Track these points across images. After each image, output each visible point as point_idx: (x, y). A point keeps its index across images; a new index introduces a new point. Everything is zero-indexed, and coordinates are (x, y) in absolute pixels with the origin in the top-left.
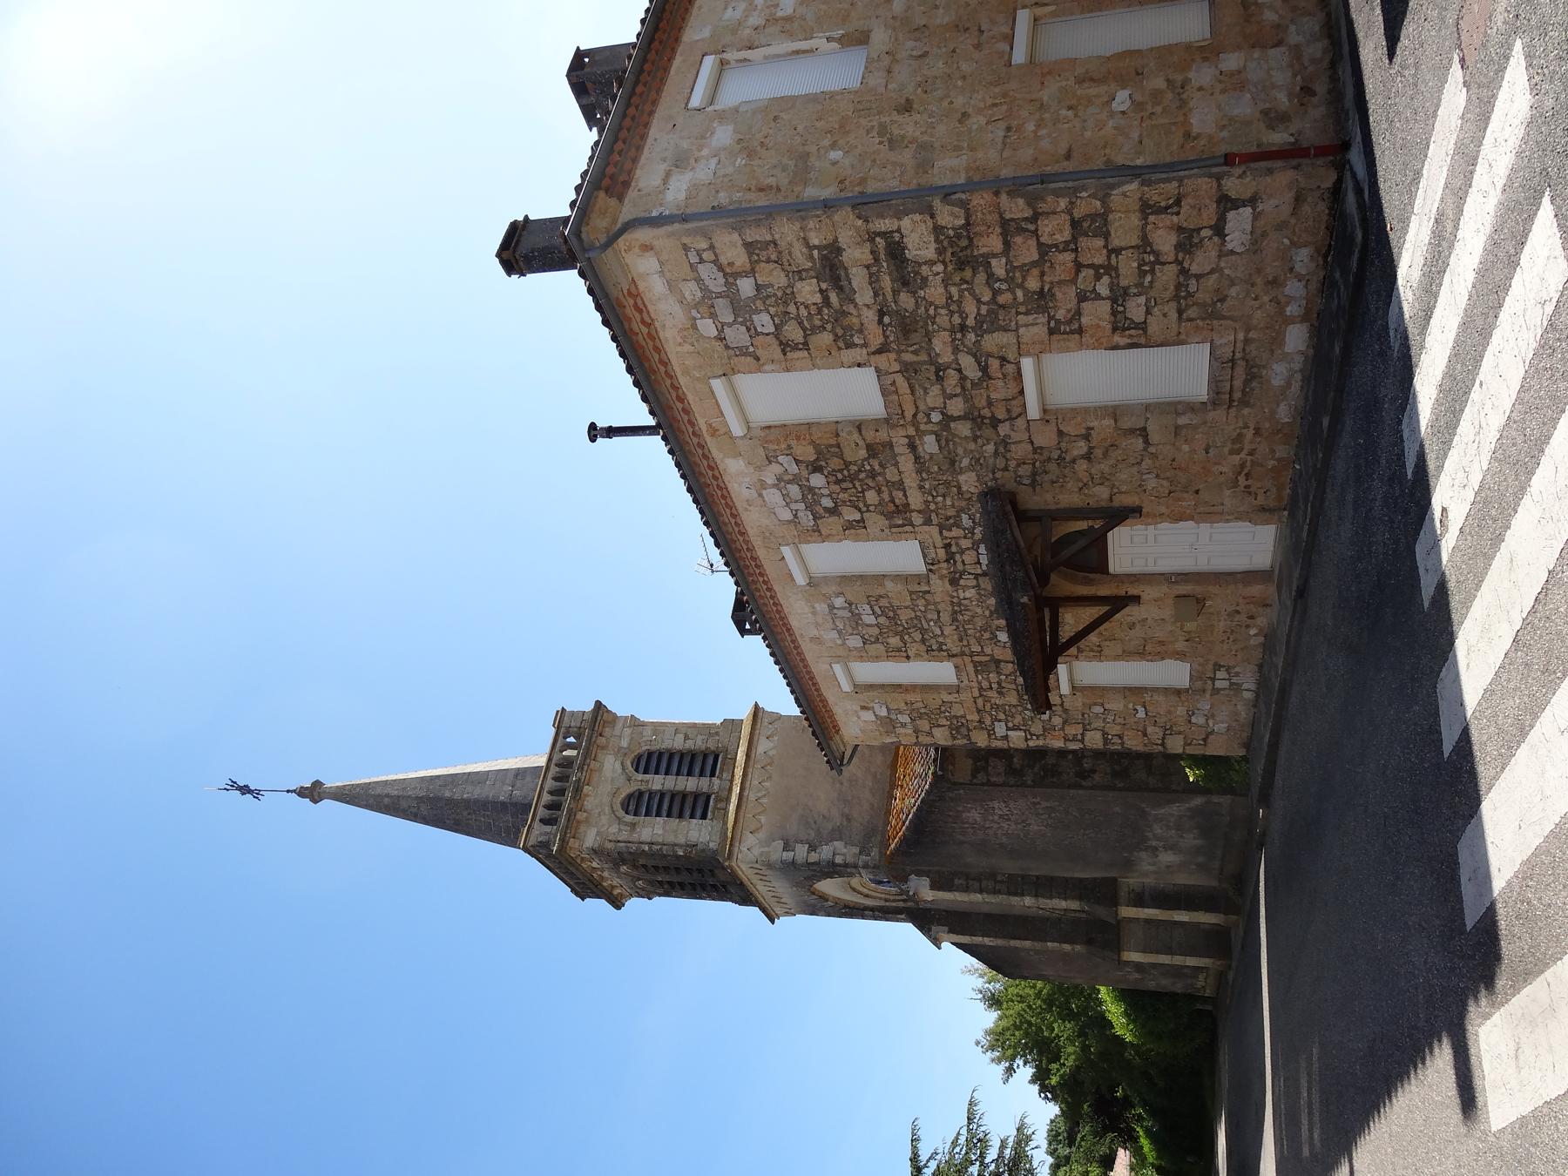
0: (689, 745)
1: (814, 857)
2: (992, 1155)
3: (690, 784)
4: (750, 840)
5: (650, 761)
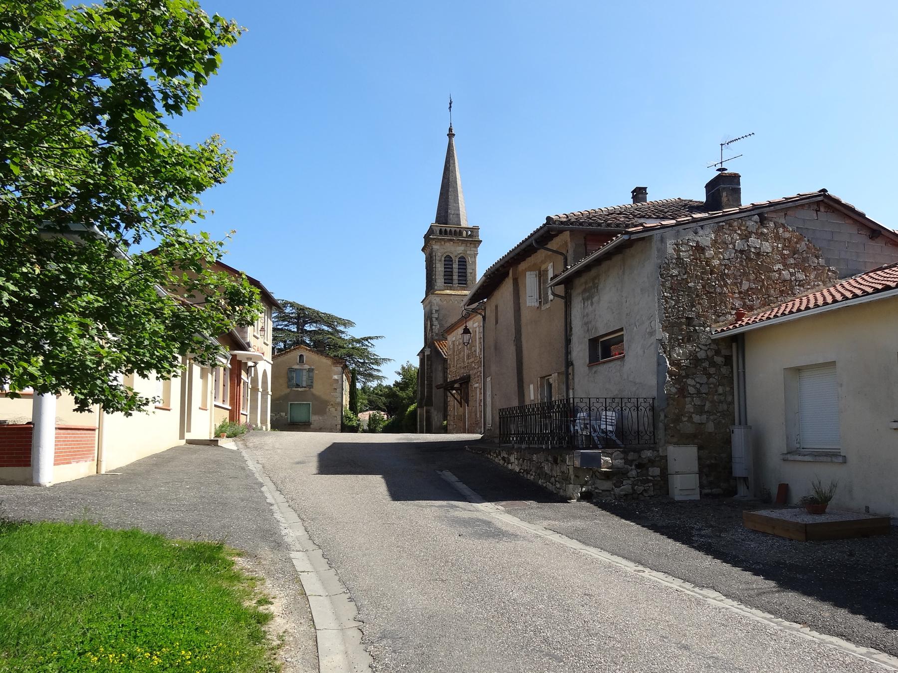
0: (469, 275)
1: (434, 319)
2: (375, 367)
3: (455, 277)
4: (438, 299)
5: (463, 262)
